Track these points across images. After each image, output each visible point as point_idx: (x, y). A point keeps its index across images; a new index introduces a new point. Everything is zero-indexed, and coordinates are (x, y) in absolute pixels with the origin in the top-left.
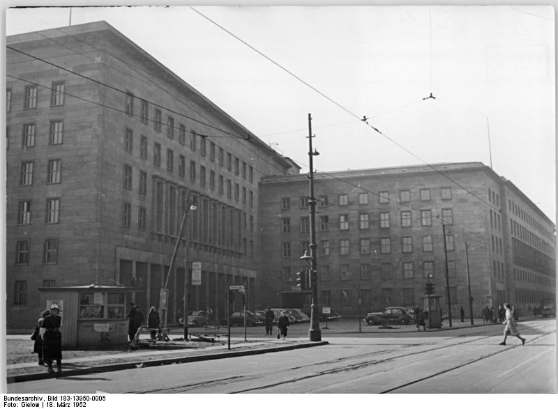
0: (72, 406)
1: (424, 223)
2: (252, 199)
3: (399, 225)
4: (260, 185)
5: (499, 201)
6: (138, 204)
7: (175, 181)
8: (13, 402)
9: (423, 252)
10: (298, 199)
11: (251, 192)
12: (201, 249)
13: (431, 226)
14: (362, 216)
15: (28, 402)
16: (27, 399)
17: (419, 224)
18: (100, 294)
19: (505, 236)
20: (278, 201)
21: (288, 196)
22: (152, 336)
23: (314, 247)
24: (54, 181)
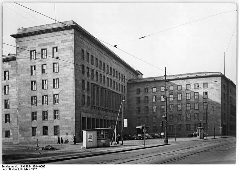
0: (31, 170)
1: (196, 98)
2: (125, 89)
3: (185, 99)
4: (128, 83)
5: (227, 89)
6: (87, 95)
7: (99, 84)
8: (6, 168)
9: (195, 109)
10: (144, 89)
11: (124, 87)
12: (107, 111)
13: (198, 99)
15: (12, 168)
16: (12, 167)
17: (193, 98)
18: (103, 131)
19: (228, 103)
20: (135, 90)
23: (167, 113)
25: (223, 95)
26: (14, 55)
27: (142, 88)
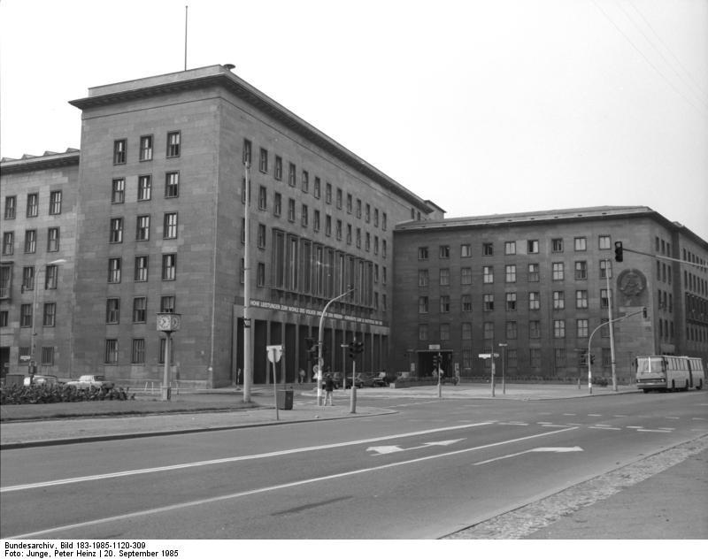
4: (395, 233)
8: (17, 550)
11: (384, 242)
14: (508, 268)
16: (35, 546)
21: (424, 245)
22: (392, 382)
24: (170, 236)
25: (659, 269)
26: (78, 151)
27: (434, 246)
